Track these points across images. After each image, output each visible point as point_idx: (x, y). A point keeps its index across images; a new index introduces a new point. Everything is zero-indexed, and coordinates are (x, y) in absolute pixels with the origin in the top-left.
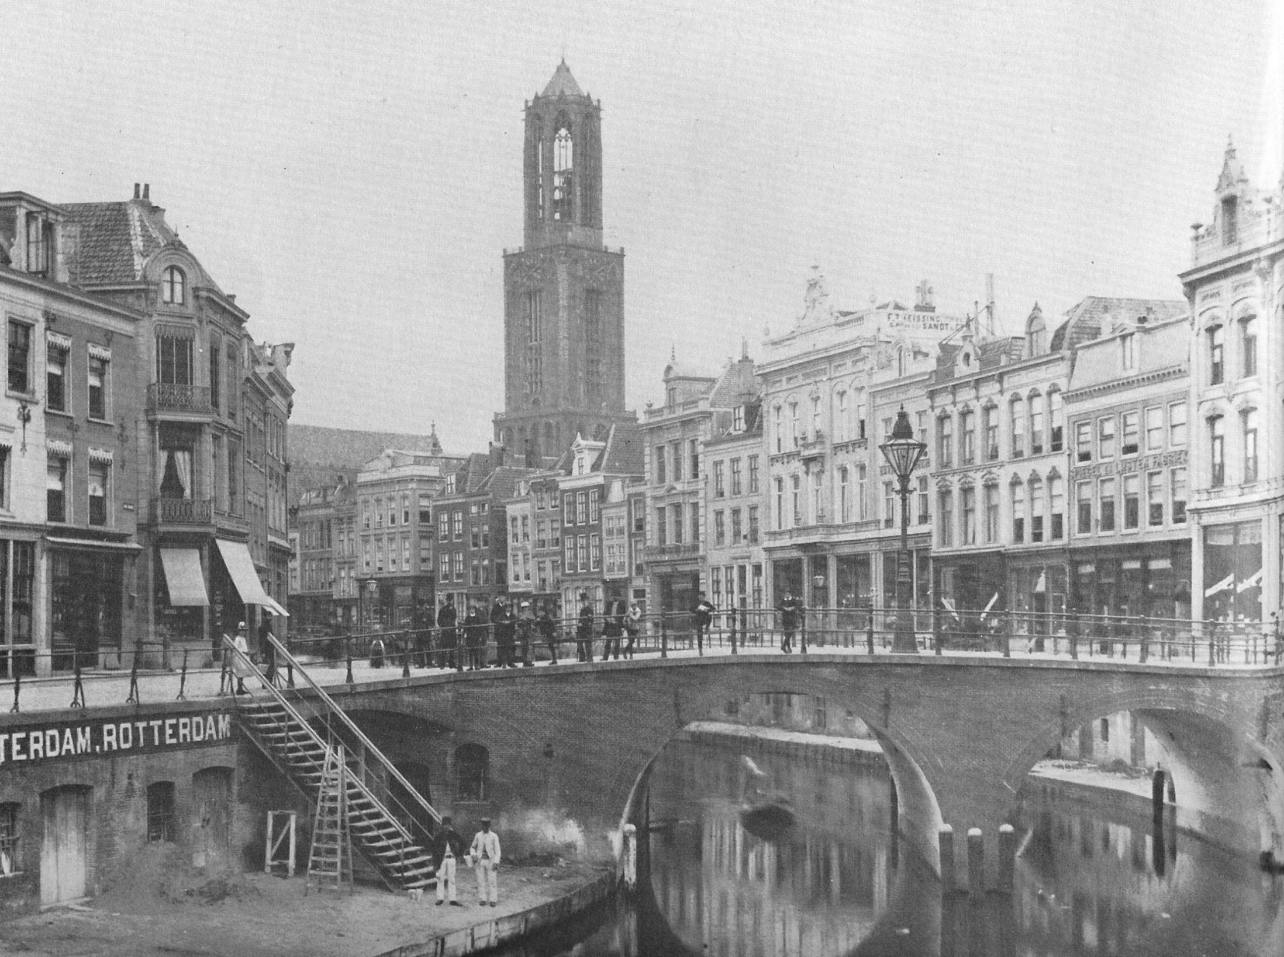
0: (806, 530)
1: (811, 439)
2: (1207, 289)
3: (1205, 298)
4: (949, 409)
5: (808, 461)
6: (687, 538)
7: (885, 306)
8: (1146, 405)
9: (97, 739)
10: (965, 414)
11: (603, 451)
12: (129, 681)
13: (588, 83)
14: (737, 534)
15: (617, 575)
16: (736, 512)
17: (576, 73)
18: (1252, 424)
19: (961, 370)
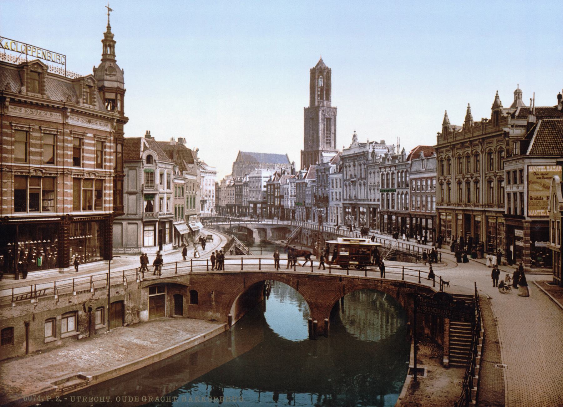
0: (352, 200)
1: (353, 176)
2: (489, 140)
3: (487, 143)
4: (395, 171)
5: (352, 182)
6: (502, 202)
7: (372, 143)
8: (421, 179)
9: (119, 153)
10: (393, 174)
11: (307, 173)
12: (367, 272)
13: (328, 64)
14: (336, 199)
15: (309, 206)
16: (336, 193)
17: (324, 61)
18: (492, 185)
19: (387, 163)
